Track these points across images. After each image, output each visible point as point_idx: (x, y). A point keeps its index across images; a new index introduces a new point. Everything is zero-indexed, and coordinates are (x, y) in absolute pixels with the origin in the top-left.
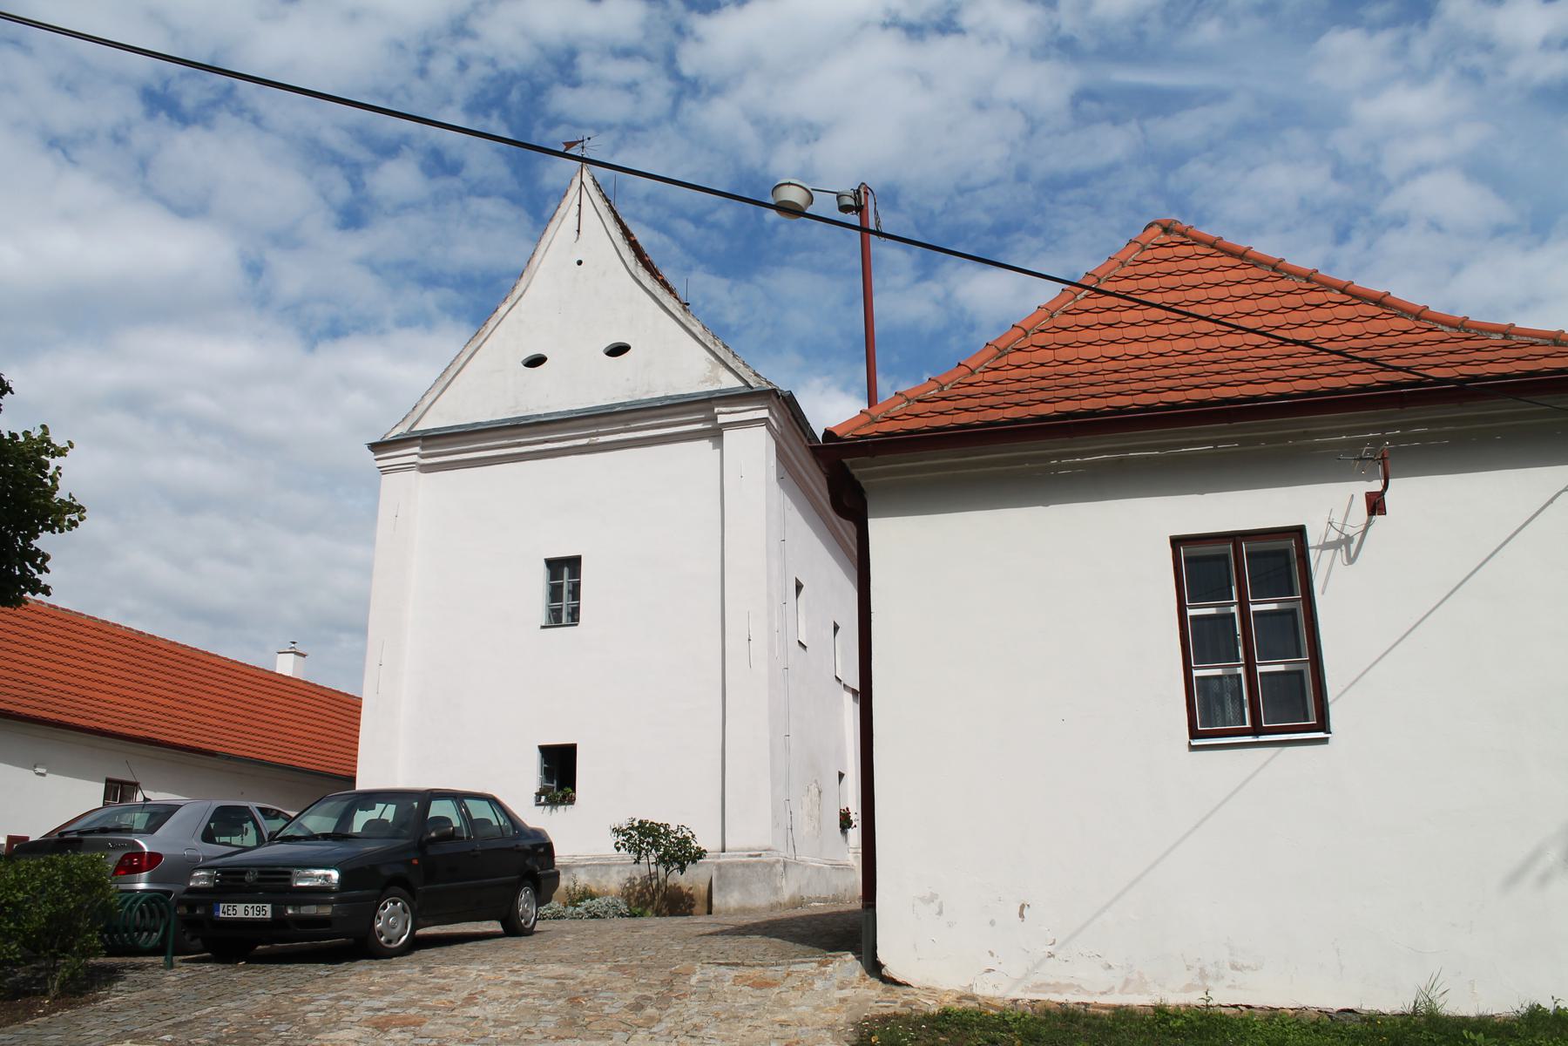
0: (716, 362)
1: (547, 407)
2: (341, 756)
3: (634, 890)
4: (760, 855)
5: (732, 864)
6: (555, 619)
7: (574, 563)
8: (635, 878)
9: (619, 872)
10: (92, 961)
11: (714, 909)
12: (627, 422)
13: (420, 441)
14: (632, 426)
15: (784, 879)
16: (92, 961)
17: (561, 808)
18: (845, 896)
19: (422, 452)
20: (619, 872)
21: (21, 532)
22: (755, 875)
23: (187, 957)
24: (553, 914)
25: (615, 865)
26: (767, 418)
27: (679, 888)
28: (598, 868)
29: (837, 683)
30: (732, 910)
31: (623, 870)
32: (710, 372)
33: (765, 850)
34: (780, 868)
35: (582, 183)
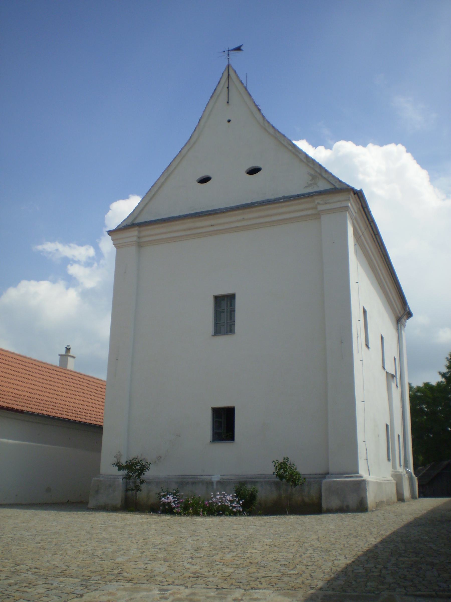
2: (95, 413)
6: (217, 332)
7: (231, 297)
10: (212, 520)
16: (212, 520)
23: (358, 479)
29: (382, 370)
30: (223, 514)
35: (229, 75)
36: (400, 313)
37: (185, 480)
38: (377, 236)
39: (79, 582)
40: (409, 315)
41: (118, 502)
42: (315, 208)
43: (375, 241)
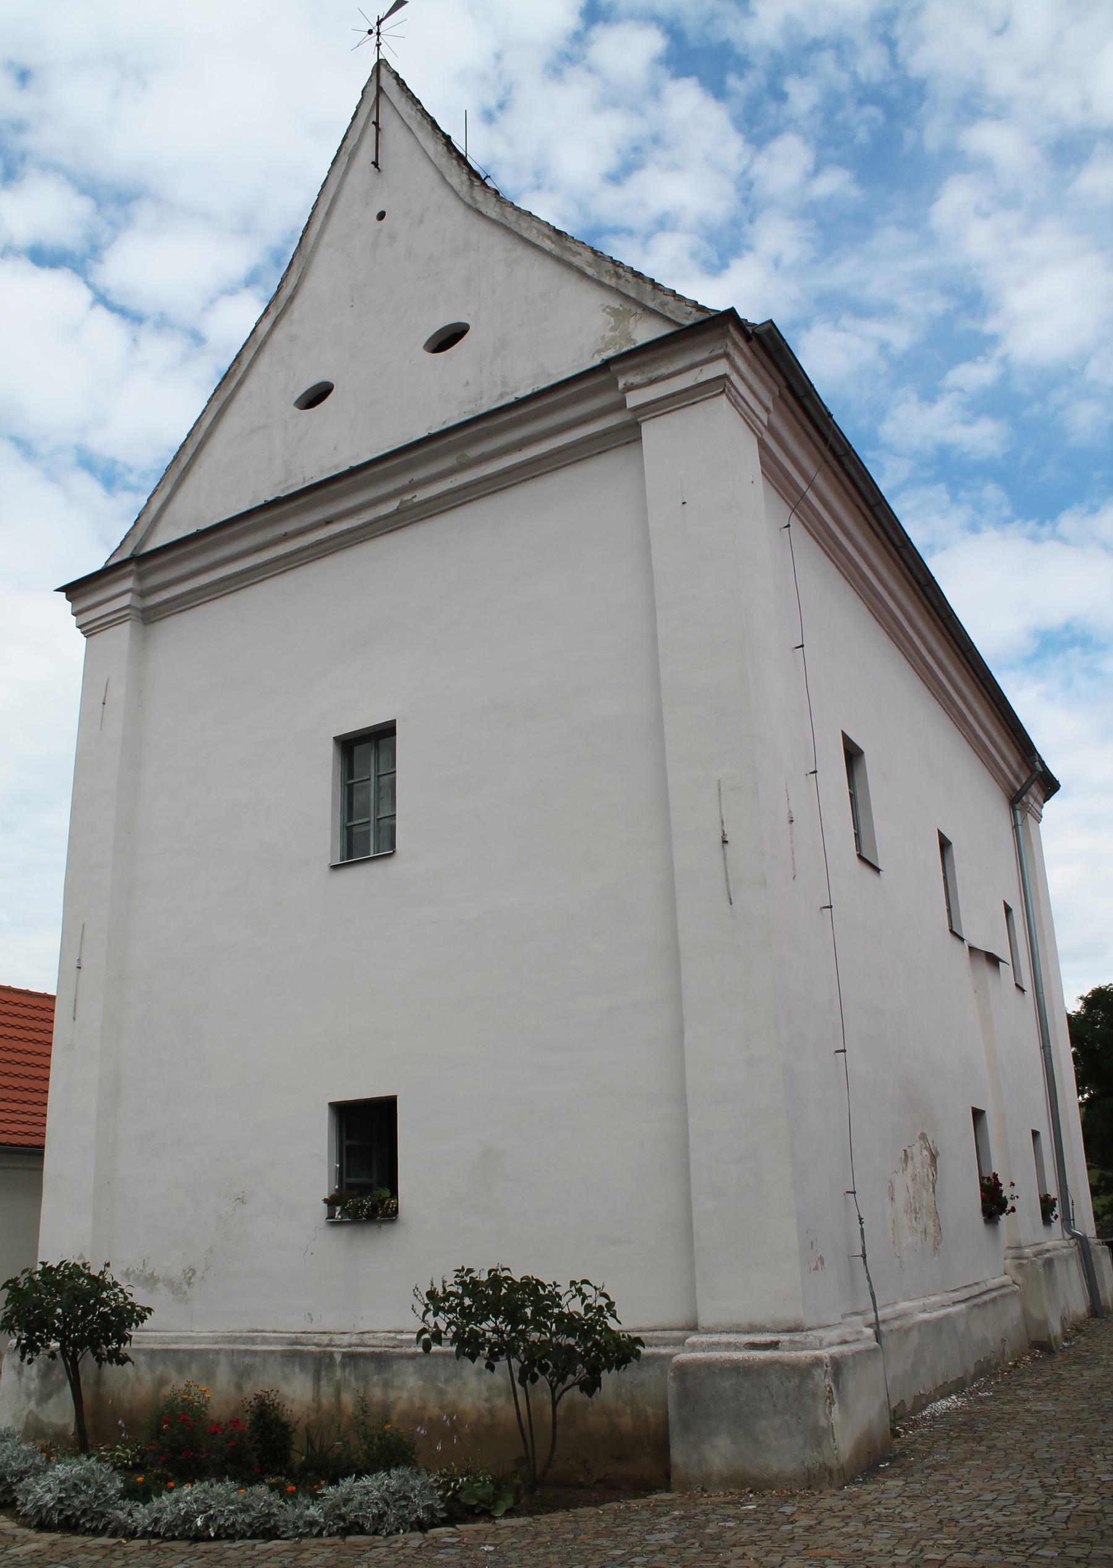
4: (774, 1345)
5: (710, 1368)
7: (385, 733)
11: (674, 1476)
13: (132, 567)
15: (835, 1408)
18: (1003, 1353)
24: (250, 1525)
26: (725, 377)
28: (440, 1361)
32: (612, 330)
33: (789, 1331)
34: (823, 1380)
36: (1017, 778)
37: (168, 1334)
38: (877, 510)
39: (123, 1565)
40: (1050, 786)
41: (983, 1175)
42: (621, 405)
43: (878, 536)
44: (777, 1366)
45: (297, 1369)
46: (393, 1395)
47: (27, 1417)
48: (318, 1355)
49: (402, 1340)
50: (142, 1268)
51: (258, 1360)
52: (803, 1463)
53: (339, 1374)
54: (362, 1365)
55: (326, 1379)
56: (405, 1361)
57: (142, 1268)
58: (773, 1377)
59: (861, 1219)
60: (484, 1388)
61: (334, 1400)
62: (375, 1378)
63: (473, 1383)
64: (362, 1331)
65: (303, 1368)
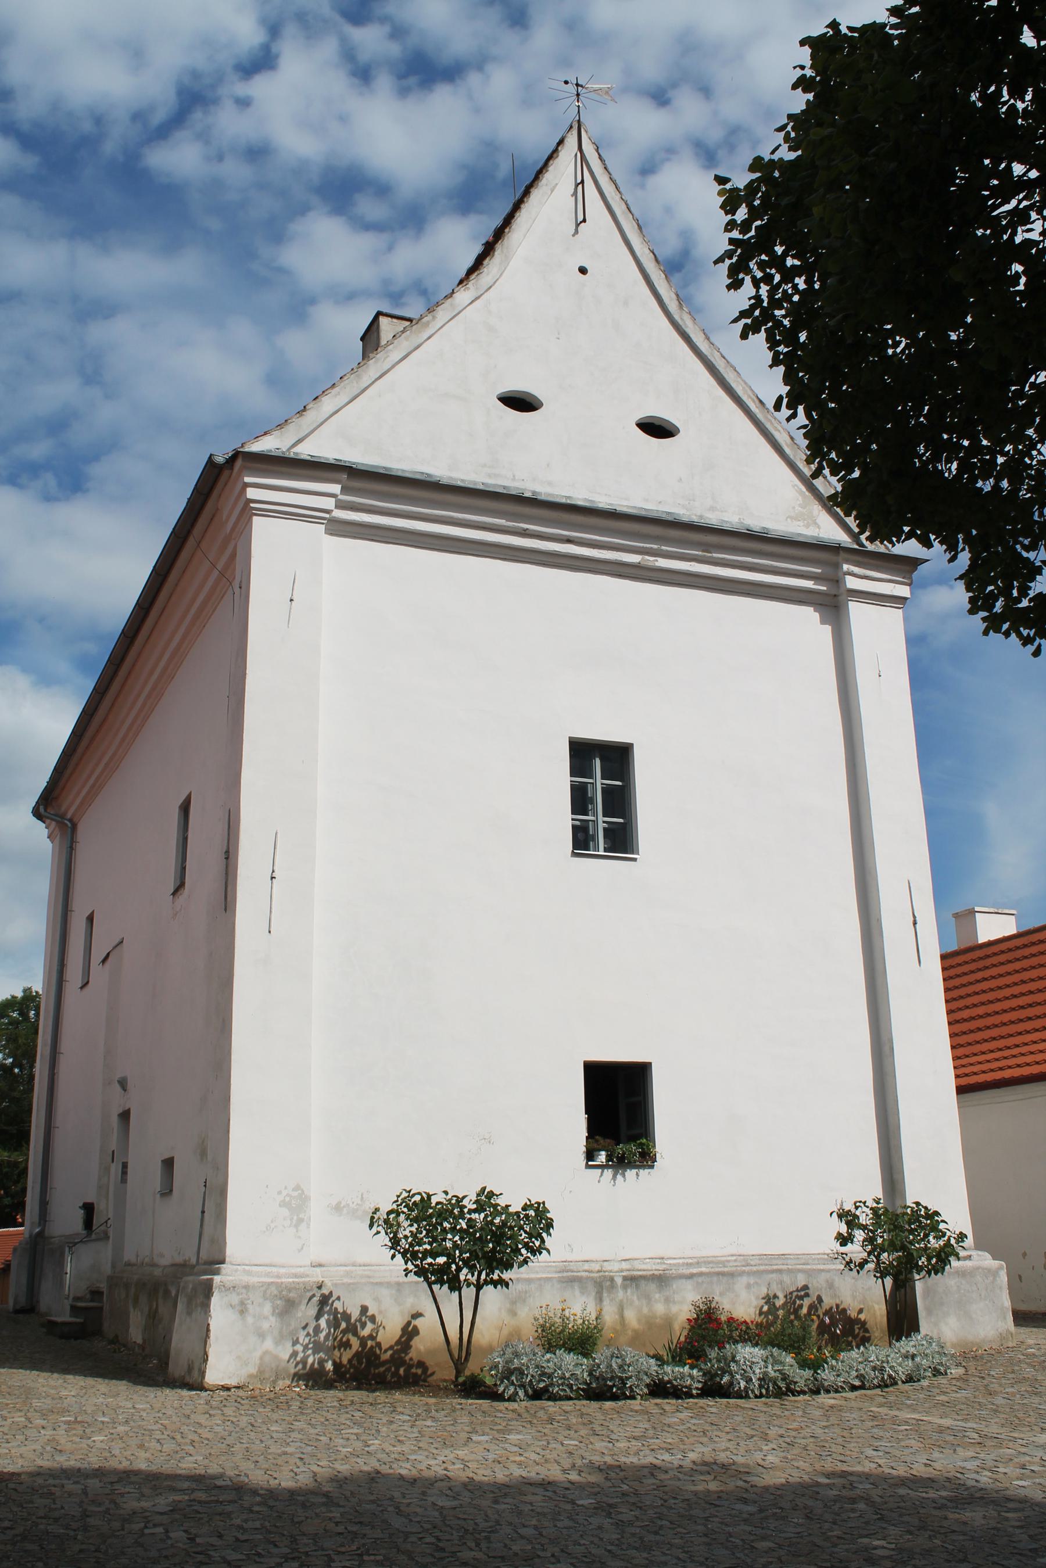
0: (807, 493)
1: (550, 484)
3: (776, 1317)
8: (775, 1296)
9: (748, 1286)
12: (707, 547)
14: (715, 555)
17: (631, 1173)
19: (341, 497)
20: (748, 1286)
21: (955, 440)
22: (974, 1288)
25: (742, 1274)
27: (844, 1310)
28: (715, 1279)
31: (756, 1283)
44: (980, 1270)
45: (577, 1292)
46: (675, 1309)
47: (261, 1358)
48: (598, 1280)
49: (670, 1264)
50: (359, 1202)
51: (533, 1286)
52: (997, 1330)
53: (621, 1294)
54: (644, 1285)
55: (608, 1299)
56: (684, 1281)
57: (359, 1202)
58: (978, 1277)
59: (205, 1186)
60: (753, 1298)
61: (617, 1317)
62: (657, 1296)
63: (744, 1294)
64: (624, 1258)
65: (583, 1290)
